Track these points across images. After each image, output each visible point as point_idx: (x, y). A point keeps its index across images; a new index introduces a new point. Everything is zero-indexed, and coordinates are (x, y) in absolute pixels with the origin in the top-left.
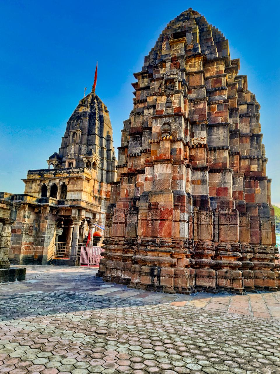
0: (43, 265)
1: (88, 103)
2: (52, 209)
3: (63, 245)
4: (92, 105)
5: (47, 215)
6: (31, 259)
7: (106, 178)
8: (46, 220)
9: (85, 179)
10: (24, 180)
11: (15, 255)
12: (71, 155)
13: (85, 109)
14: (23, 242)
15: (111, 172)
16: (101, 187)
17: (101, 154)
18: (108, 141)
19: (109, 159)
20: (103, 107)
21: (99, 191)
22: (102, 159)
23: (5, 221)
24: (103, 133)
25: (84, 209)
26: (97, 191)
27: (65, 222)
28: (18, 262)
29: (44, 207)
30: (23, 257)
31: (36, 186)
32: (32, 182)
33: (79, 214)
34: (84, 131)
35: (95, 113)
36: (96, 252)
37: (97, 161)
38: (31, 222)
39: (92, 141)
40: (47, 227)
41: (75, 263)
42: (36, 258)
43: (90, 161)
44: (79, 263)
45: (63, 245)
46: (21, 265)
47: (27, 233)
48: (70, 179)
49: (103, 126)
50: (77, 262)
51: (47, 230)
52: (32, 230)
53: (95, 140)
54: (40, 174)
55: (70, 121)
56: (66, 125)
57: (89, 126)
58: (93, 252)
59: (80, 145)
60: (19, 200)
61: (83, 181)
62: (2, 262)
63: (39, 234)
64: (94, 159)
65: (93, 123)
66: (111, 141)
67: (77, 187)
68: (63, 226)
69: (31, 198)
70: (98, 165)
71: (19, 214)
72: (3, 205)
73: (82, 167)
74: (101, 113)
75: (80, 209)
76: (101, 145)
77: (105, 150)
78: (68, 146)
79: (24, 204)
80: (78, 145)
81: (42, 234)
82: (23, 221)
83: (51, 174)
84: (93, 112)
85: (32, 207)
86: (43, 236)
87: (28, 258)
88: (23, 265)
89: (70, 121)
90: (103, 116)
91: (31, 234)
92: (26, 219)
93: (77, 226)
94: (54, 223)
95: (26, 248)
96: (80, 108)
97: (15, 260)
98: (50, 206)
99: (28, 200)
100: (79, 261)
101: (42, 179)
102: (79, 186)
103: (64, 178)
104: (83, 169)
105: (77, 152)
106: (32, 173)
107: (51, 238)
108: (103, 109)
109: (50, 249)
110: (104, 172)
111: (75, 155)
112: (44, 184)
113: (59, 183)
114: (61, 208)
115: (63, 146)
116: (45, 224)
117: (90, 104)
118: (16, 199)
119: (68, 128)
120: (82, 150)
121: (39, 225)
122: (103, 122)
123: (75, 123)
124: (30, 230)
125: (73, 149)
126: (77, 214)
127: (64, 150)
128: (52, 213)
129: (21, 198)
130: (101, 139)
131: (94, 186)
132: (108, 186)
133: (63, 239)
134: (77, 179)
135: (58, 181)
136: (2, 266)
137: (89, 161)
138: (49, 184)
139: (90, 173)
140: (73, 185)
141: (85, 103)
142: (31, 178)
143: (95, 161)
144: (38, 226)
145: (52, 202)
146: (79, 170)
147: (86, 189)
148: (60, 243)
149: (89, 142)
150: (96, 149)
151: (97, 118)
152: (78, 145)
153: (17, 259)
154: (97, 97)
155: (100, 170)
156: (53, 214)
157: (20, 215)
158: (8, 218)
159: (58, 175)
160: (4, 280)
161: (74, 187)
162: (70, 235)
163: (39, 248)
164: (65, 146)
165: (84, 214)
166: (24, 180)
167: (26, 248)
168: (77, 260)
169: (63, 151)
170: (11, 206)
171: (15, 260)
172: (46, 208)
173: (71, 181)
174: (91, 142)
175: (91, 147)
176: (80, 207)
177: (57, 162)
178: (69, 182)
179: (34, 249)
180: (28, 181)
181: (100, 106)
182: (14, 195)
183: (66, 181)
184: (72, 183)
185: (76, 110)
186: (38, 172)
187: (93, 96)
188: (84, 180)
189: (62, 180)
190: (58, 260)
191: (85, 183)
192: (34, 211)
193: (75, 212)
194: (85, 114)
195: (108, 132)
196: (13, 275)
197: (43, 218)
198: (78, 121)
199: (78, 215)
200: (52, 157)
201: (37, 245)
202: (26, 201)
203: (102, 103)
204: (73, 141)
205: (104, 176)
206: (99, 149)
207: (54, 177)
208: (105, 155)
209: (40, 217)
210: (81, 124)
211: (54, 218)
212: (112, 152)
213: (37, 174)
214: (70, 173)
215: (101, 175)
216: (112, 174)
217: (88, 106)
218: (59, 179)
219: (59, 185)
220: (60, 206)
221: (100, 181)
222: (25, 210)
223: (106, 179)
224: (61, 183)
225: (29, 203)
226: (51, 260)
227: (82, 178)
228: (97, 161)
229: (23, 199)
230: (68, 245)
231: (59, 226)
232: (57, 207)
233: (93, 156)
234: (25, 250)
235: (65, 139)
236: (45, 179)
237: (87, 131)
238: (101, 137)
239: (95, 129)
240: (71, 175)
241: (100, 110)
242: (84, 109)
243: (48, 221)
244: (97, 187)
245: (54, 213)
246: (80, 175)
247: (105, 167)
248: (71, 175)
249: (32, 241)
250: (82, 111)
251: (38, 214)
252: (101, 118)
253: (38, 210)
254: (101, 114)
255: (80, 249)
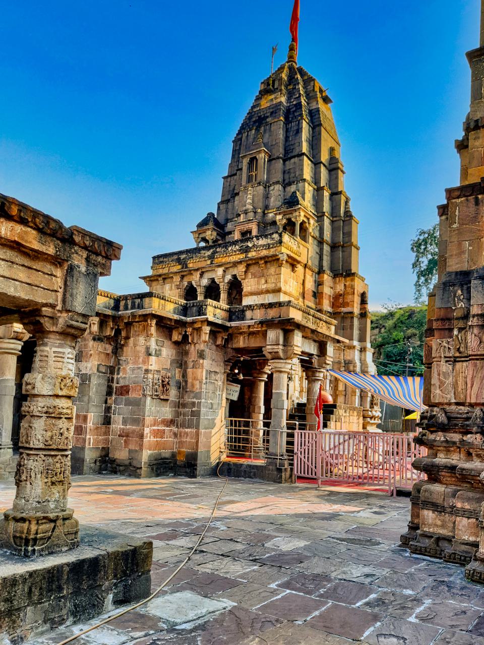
0: (199, 479)
1: (280, 85)
2: (216, 329)
3: (242, 424)
4: (291, 87)
5: (202, 347)
6: (170, 462)
7: (329, 262)
8: (201, 361)
9: (287, 261)
10: (144, 278)
11: (130, 451)
12: (246, 214)
13: (276, 98)
14: (148, 420)
15: (343, 247)
16: (319, 284)
17: (318, 202)
18: (333, 173)
19: (336, 217)
20: (317, 89)
21: (317, 295)
22: (320, 217)
23: (42, 320)
24: (320, 152)
25: (299, 326)
26: (311, 294)
27: (247, 368)
28: (138, 471)
29: (196, 326)
30: (150, 456)
31: (171, 289)
32: (164, 282)
33: (287, 343)
34: (274, 151)
35: (299, 106)
36: (341, 447)
37: (308, 219)
38: (164, 367)
39: (295, 172)
40: (204, 378)
41: (283, 474)
42: (181, 459)
43: (293, 220)
44: (291, 476)
45: (242, 424)
46: (146, 477)
47: (157, 395)
48: (250, 264)
49: (320, 134)
50: (288, 473)
51: (204, 386)
52: (168, 387)
53: (302, 170)
54: (179, 261)
55: (240, 136)
56: (230, 147)
57: (287, 138)
58: (332, 446)
59: (265, 188)
60: (132, 308)
61: (280, 266)
62: (38, 520)
63: (186, 397)
64: (302, 214)
65: (295, 128)
66: (340, 172)
67: (266, 282)
68: (241, 377)
69: (162, 302)
70: (311, 230)
71: (135, 345)
72: (19, 228)
73: (277, 232)
74: (315, 103)
75: (288, 327)
76: (316, 180)
77: (326, 194)
78: (237, 194)
79: (145, 317)
80: (261, 187)
81: (193, 398)
82: (144, 362)
83: (204, 257)
84: (294, 103)
85: (165, 325)
86: (197, 401)
87: (162, 459)
88: (150, 477)
89: (240, 136)
90: (318, 110)
91: (166, 397)
92: (153, 359)
93: (282, 374)
94: (220, 369)
95: (157, 433)
96: (263, 99)
97: (130, 464)
98: (210, 323)
99: (155, 306)
100: (292, 470)
101: (185, 272)
102: (272, 280)
103: (235, 264)
104: (280, 235)
105: (261, 204)
106: (163, 262)
107: (215, 407)
108: (319, 95)
109: (215, 441)
110: (326, 248)
111: (255, 213)
112: (190, 283)
113: (224, 276)
114: (237, 328)
115: (226, 198)
116: (200, 370)
117: (286, 86)
118: (126, 308)
119: (236, 153)
120: (272, 199)
121: (184, 375)
122: (320, 125)
123: (252, 137)
124: (163, 386)
125: (249, 198)
126: (281, 341)
127: (230, 204)
128: (215, 342)
129: (136, 304)
130: (315, 168)
131: (304, 281)
132: (335, 283)
133: (239, 409)
134: (266, 262)
135: (220, 271)
136: (35, 540)
137: (289, 220)
138: (201, 283)
139: (295, 248)
140: (256, 279)
141: (273, 86)
142: (161, 272)
143: (306, 220)
144: (183, 376)
145: (215, 311)
146: (269, 241)
147: (288, 287)
148: (235, 421)
149: (287, 176)
150: (307, 191)
151: (304, 117)
152: (261, 187)
153: (135, 463)
154: (301, 71)
155: (316, 242)
156: (217, 346)
157: (138, 348)
158: (53, 306)
159: (220, 259)
160: (45, 622)
161: (258, 283)
162: (259, 402)
163: (187, 434)
164: (230, 195)
165: (299, 342)
166: (144, 278)
167: (157, 433)
168: (286, 466)
169: (227, 208)
170: (63, 240)
171: (130, 464)
172: (199, 330)
173: (253, 269)
174: (292, 175)
175: (293, 188)
176: (290, 321)
177: (215, 233)
178: (246, 272)
179: (175, 435)
180: (154, 280)
181: (310, 88)
182: (120, 297)
183: (240, 270)
184: (254, 276)
185: (253, 107)
186: (175, 257)
187: (291, 68)
188: (284, 262)
189: (231, 270)
190: (235, 464)
191: (285, 270)
192: (170, 337)
193: (274, 338)
194: (275, 110)
195: (332, 150)
196: (91, 587)
197: (193, 356)
198: (259, 131)
199: (284, 346)
200: (203, 224)
201: (183, 425)
202: (147, 311)
203: (314, 80)
204: (249, 179)
205: (325, 258)
206: (312, 192)
207: (211, 263)
208: (326, 207)
209: (186, 353)
210: (267, 135)
211: (219, 356)
212: (343, 199)
213: (172, 261)
214: (247, 250)
215: (318, 257)
216: (346, 253)
217: (281, 90)
218: (223, 268)
219: (223, 282)
220: (233, 324)
221: (317, 270)
222: (149, 336)
223: (329, 266)
224: (228, 277)
225: (159, 314)
226: (218, 464)
227: (278, 259)
228: (308, 219)
229: (141, 307)
230: (255, 424)
231: (232, 379)
232: (228, 324)
233: (299, 206)
234: (152, 439)
235: (229, 179)
236: (190, 271)
237: (281, 150)
238: (316, 163)
239: (300, 144)
240: (250, 255)
241: (310, 97)
242: (272, 100)
243: (207, 363)
244: (310, 285)
245: (219, 342)
246: (272, 252)
247: (327, 236)
248: (252, 254)
249: (169, 416)
250: (268, 105)
251: (182, 345)
252: (314, 115)
253: (180, 334)
254: (313, 106)
255: (290, 435)
